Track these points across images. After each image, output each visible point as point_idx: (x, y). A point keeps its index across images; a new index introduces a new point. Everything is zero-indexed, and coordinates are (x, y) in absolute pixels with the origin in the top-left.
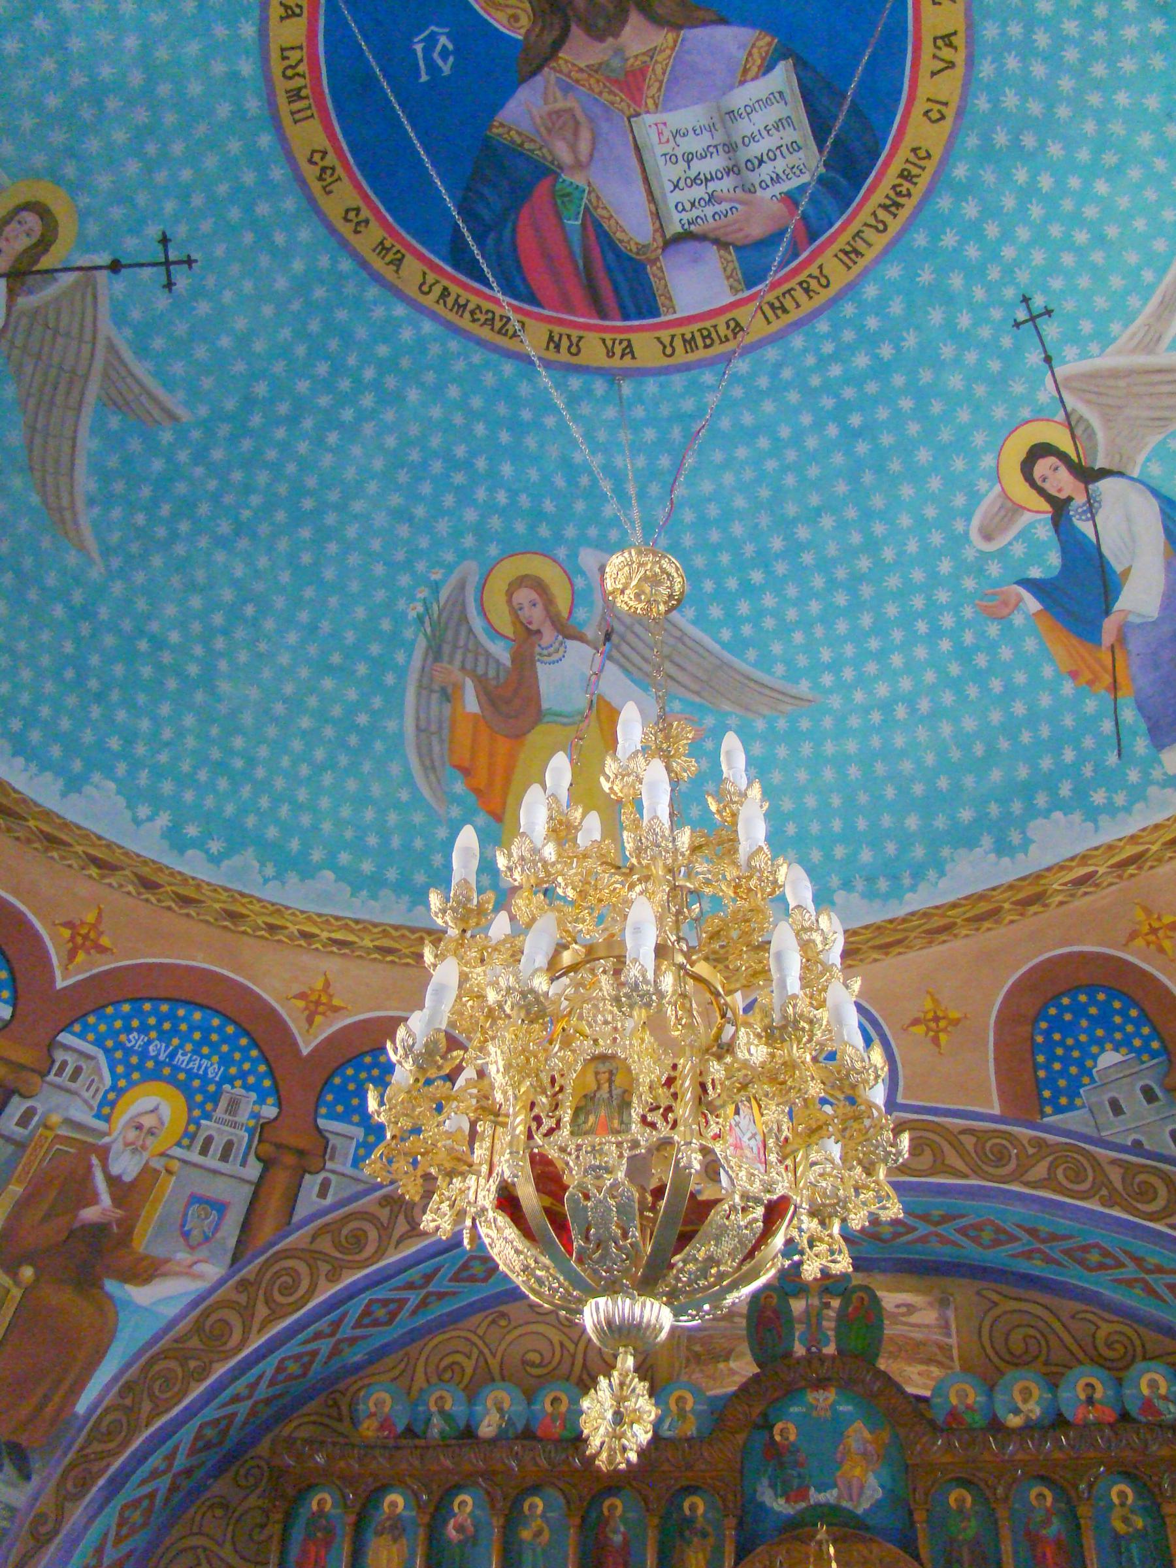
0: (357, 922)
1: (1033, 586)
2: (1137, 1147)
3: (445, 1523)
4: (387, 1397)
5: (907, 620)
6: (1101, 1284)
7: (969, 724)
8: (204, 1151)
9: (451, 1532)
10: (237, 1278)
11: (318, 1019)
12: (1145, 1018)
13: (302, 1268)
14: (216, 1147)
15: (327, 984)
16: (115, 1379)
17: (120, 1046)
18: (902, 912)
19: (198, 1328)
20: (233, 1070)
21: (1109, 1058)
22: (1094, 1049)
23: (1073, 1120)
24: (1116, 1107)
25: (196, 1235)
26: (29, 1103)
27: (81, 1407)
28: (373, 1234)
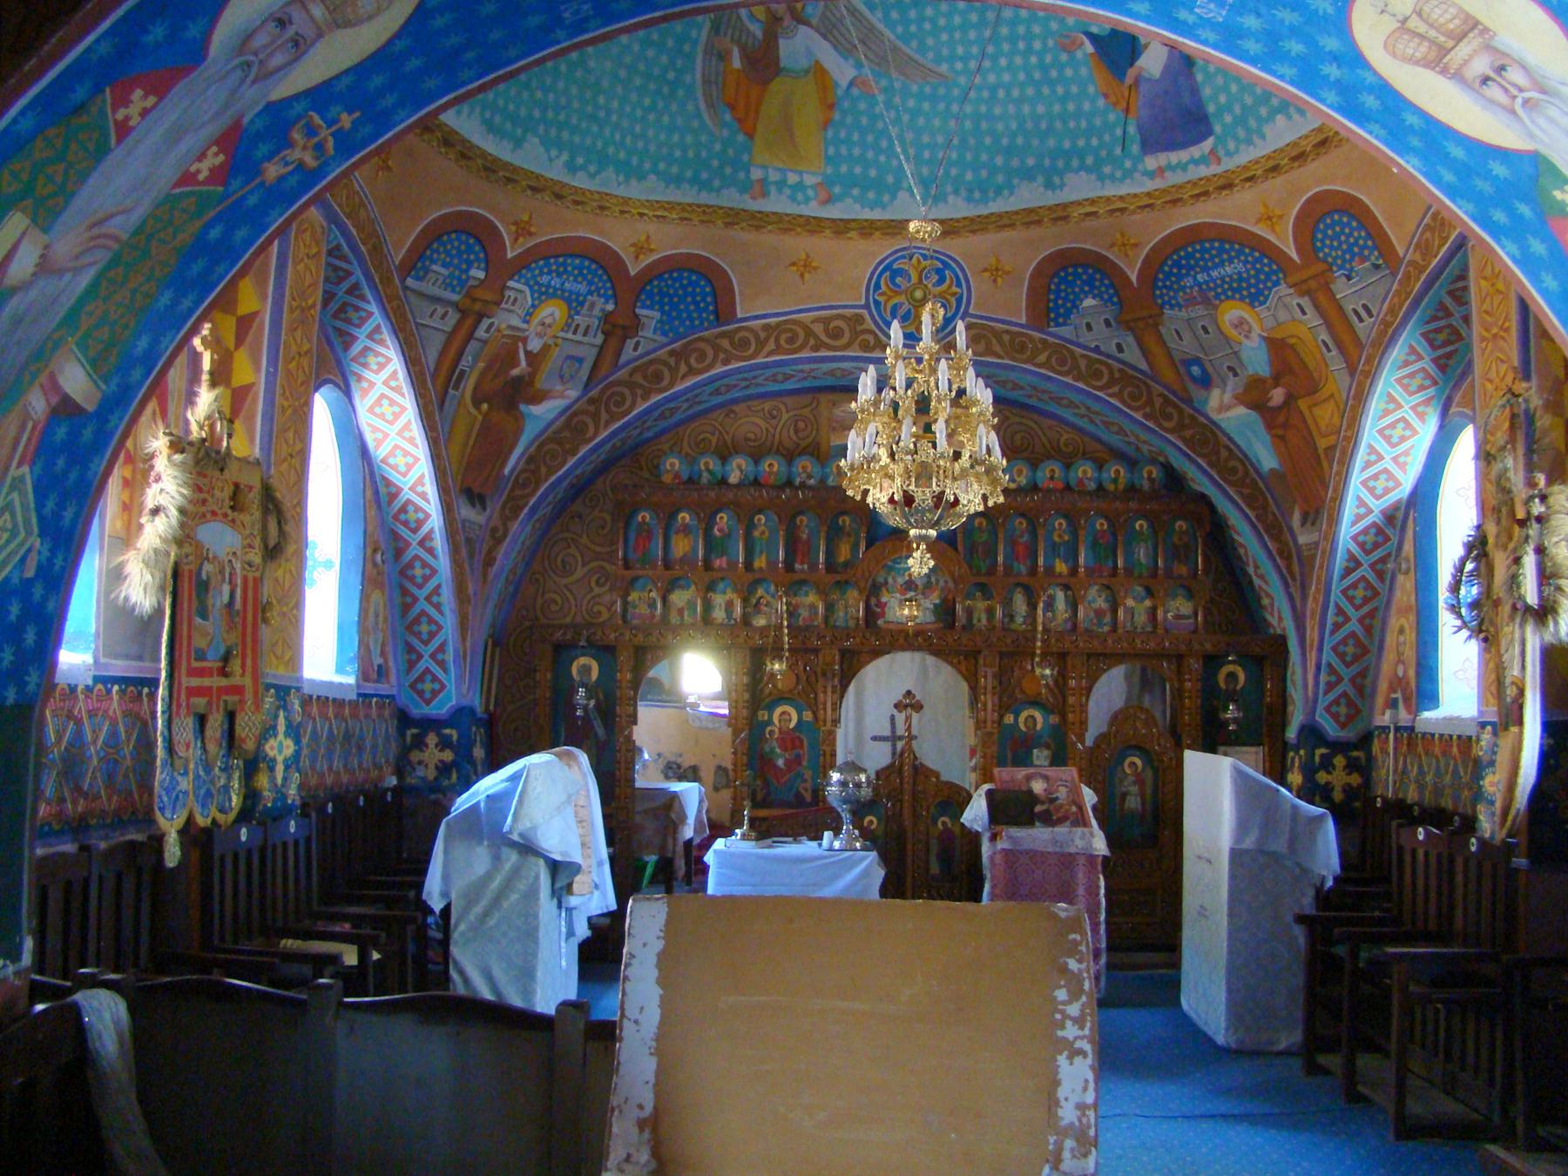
0: (668, 203)
1: (1093, 38)
2: (1097, 349)
3: (712, 528)
4: (677, 462)
5: (1013, 39)
6: (1066, 414)
7: (1040, 109)
8: (575, 333)
9: (716, 532)
10: (586, 398)
11: (642, 257)
12: (1112, 285)
13: (627, 392)
14: (581, 330)
15: (648, 237)
16: (523, 454)
17: (537, 283)
18: (985, 212)
19: (567, 425)
20: (593, 288)
21: (1089, 302)
22: (1082, 296)
23: (1064, 331)
24: (1089, 327)
25: (567, 376)
26: (490, 321)
27: (507, 471)
28: (666, 373)
